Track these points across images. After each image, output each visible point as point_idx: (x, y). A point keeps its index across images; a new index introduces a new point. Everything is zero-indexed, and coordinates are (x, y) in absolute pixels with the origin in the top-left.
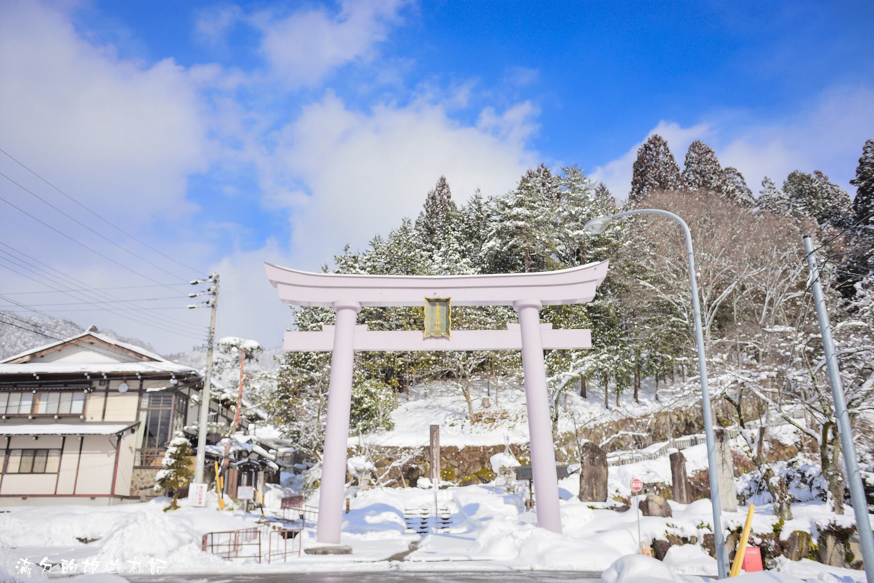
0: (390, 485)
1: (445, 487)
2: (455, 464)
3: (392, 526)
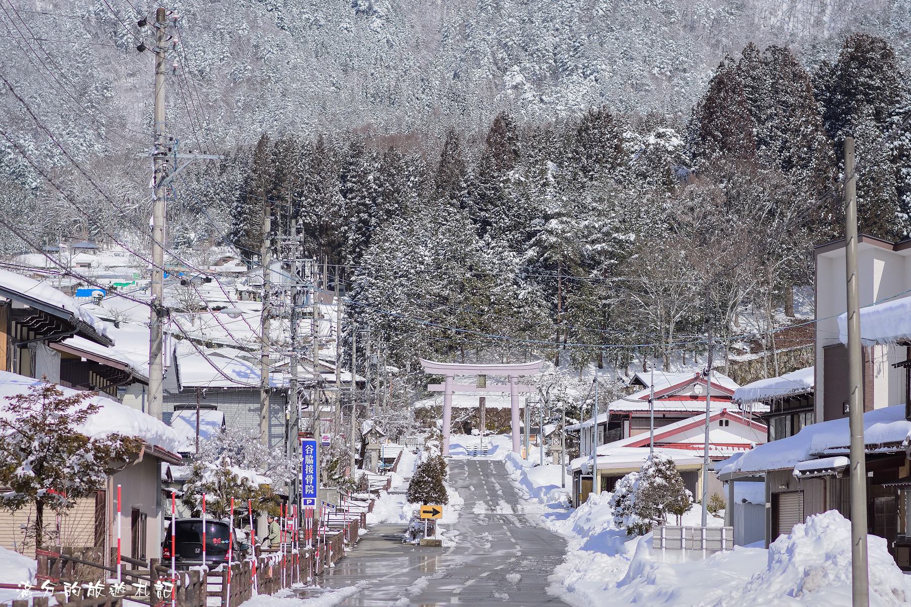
1: (487, 435)
3: (462, 453)
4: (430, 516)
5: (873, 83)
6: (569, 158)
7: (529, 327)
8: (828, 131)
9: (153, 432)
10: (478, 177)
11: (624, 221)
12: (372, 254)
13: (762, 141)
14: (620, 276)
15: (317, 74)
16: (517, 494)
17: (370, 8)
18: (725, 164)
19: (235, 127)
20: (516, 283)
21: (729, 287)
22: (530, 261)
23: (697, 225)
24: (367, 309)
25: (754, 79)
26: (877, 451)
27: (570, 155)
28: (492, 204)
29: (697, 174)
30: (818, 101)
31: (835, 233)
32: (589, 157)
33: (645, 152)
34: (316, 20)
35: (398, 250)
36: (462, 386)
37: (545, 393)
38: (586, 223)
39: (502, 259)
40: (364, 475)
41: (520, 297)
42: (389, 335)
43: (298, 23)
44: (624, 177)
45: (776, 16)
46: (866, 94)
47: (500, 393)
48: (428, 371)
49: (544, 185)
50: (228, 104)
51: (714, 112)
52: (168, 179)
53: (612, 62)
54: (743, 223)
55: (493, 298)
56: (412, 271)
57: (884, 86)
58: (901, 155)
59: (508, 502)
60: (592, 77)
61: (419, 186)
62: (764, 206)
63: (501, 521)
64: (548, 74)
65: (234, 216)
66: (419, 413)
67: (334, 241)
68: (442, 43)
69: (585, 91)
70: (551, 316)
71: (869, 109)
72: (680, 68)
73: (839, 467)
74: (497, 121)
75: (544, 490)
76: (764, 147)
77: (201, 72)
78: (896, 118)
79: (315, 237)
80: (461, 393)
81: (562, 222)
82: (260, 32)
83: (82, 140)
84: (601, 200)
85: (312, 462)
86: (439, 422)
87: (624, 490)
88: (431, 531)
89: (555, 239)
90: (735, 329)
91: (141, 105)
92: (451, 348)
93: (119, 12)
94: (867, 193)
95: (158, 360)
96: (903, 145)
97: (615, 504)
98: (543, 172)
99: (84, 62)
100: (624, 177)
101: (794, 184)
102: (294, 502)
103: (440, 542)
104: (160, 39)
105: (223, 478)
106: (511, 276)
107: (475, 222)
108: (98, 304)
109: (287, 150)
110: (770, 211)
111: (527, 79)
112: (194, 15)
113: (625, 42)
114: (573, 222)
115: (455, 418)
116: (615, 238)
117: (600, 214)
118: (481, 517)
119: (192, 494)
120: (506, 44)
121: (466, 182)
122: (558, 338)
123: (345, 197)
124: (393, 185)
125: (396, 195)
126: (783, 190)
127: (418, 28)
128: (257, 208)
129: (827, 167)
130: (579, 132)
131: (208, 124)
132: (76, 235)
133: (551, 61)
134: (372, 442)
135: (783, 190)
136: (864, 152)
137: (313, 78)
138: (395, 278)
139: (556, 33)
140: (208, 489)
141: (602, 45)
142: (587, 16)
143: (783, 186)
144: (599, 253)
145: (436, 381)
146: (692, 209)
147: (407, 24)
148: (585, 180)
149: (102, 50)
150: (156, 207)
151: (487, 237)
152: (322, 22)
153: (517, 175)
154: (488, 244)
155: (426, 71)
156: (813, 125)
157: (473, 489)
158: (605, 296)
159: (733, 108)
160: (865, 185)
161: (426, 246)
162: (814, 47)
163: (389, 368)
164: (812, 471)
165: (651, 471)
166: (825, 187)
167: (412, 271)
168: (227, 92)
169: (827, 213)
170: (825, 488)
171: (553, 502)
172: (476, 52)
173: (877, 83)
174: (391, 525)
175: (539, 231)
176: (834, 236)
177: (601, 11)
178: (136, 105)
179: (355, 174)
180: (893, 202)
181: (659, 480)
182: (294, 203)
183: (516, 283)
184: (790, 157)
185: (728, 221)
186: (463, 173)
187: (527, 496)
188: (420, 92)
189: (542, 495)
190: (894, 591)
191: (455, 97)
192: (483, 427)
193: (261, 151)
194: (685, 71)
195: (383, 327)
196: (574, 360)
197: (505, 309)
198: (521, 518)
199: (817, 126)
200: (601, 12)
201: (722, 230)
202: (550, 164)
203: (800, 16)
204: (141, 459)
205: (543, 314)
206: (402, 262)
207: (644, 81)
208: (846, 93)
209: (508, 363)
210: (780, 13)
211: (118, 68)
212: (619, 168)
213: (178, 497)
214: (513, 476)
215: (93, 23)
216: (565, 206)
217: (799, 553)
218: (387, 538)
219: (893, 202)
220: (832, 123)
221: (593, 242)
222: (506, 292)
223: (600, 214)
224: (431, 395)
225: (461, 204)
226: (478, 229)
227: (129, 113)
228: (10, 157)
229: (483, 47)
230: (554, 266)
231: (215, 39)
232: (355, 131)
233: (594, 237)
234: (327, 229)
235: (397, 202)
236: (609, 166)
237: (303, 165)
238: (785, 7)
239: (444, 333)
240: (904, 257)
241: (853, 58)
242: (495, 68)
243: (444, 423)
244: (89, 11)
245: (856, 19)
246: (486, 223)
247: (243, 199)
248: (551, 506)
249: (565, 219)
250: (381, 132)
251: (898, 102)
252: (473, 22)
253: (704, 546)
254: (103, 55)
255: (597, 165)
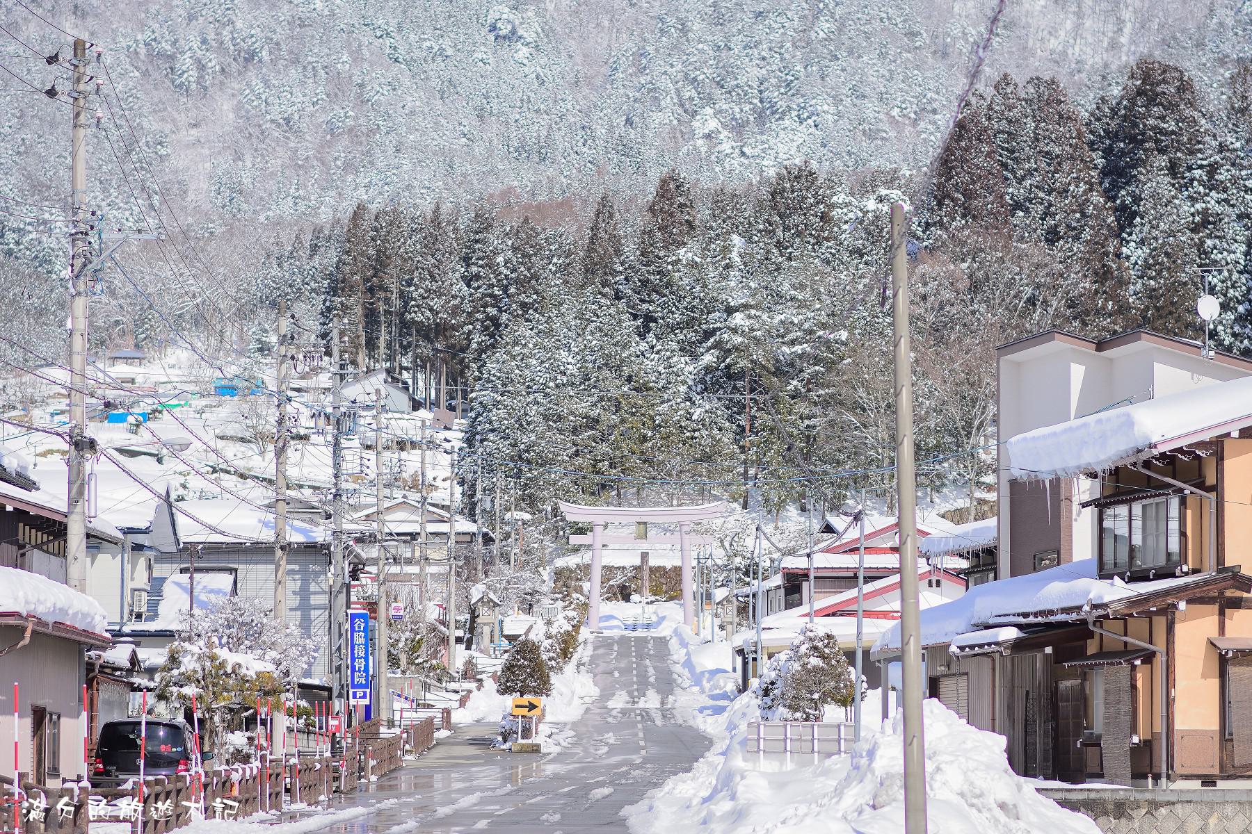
0: (608, 599)
1: (652, 602)
2: (663, 581)
4: (525, 711)
5: (1166, 126)
6: (760, 231)
7: (706, 458)
8: (1107, 191)
9: (49, 604)
10: (637, 259)
11: (833, 315)
12: (498, 362)
13: (1017, 206)
14: (828, 387)
15: (443, 122)
16: (675, 680)
17: (513, 32)
18: (968, 237)
19: (333, 194)
20: (689, 399)
21: (974, 401)
22: (708, 369)
23: (931, 318)
24: (491, 436)
25: (1010, 122)
26: (1052, 619)
27: (761, 227)
28: (657, 293)
29: (931, 250)
30: (1094, 150)
31: (1117, 328)
32: (786, 229)
33: (861, 222)
34: (442, 50)
35: (532, 355)
36: (616, 536)
37: (728, 546)
38: (782, 317)
39: (672, 367)
40: (471, 657)
41: (695, 417)
42: (521, 470)
43: (417, 54)
44: (834, 255)
45: (1056, 38)
46: (1157, 141)
47: (669, 546)
48: (570, 518)
49: (727, 267)
50: (323, 164)
51: (953, 168)
52: (90, 266)
53: (837, 100)
54: (994, 315)
55: (658, 420)
56: (552, 384)
57: (1181, 129)
58: (1205, 223)
59: (658, 692)
60: (810, 121)
61: (564, 270)
62: (1021, 292)
63: (639, 718)
64: (751, 118)
65: (322, 313)
66: (559, 574)
67: (453, 346)
68: (610, 79)
69: (801, 141)
70: (736, 441)
71: (1163, 161)
72: (929, 108)
73: (1009, 641)
74: (664, 182)
75: (707, 675)
76: (1021, 214)
77: (287, 120)
78: (1197, 173)
79: (432, 342)
80: (617, 546)
81: (750, 317)
82: (366, 66)
83: (127, 213)
84: (802, 287)
85: (363, 641)
86: (586, 586)
87: (773, 675)
88: (526, 733)
89: (740, 340)
90: (983, 457)
91: (208, 165)
92: (604, 486)
93: (176, 41)
94: (1159, 273)
95: (78, 509)
96: (1208, 209)
97: (761, 693)
98: (726, 250)
99: (130, 109)
100: (834, 255)
101: (1061, 262)
102: (340, 696)
103: (539, 746)
104: (78, 80)
105: (208, 664)
106: (683, 388)
107: (635, 317)
108: (136, 433)
109: (391, 224)
110: (1029, 300)
111: (724, 126)
112: (277, 44)
113: (855, 73)
114: (765, 317)
115: (609, 580)
116: (820, 337)
117: (801, 305)
118: (614, 713)
119: (167, 685)
120: (695, 79)
121: (622, 264)
122: (746, 472)
123: (469, 286)
124: (529, 270)
125: (534, 282)
126: (1046, 270)
127: (579, 59)
128: (352, 301)
129: (1106, 239)
130: (773, 194)
131: (297, 190)
132: (118, 341)
133: (756, 101)
134: (484, 615)
135: (1046, 270)
136: (1155, 219)
137: (437, 126)
138: (528, 393)
139: (762, 63)
140: (187, 679)
141: (823, 79)
142: (804, 41)
143: (1046, 265)
144: (801, 356)
145: (581, 531)
146: (924, 298)
147: (564, 54)
148: (781, 259)
149: (155, 93)
150: (75, 304)
151: (650, 337)
152: (450, 52)
153: (690, 255)
154: (652, 347)
155: (588, 116)
156: (1086, 183)
157: (616, 674)
158: (804, 416)
159: (980, 161)
160: (1157, 263)
161: (569, 350)
162: (1104, 78)
163: (518, 515)
164: (972, 647)
165: (803, 649)
166: (1104, 266)
167: (552, 384)
168: (322, 147)
169: (1106, 300)
170: (994, 669)
171: (717, 691)
172: (654, 90)
173: (1171, 126)
174: (489, 724)
175: (720, 329)
176: (1115, 332)
177: (821, 33)
178: (200, 166)
179: (481, 254)
180: (1195, 284)
181: (814, 661)
182: (402, 295)
183: (689, 399)
184: (1056, 226)
185: (973, 313)
186: (618, 253)
187: (686, 683)
188: (580, 144)
189: (705, 682)
190: (1002, 806)
191: (625, 149)
192: (646, 592)
193: (356, 226)
194: (934, 111)
195: (512, 459)
196: (767, 500)
197: (677, 434)
198: (666, 713)
199: (1091, 184)
200: (822, 35)
201: (965, 325)
202: (737, 240)
203: (1089, 37)
204: (27, 640)
205: (726, 440)
206: (537, 370)
207: (881, 126)
208: (1133, 139)
209: (679, 505)
210: (1062, 33)
211: (176, 115)
212: (826, 244)
213: (149, 690)
214: (675, 657)
215: (142, 57)
216: (753, 295)
217: (881, 757)
218: (474, 742)
219: (1195, 284)
220: (1113, 180)
221: (792, 343)
222: (676, 411)
223: (801, 305)
224: (576, 549)
225: (616, 293)
226: (638, 327)
227: (192, 177)
228: (31, 236)
229: (664, 83)
230: (741, 375)
231: (305, 76)
232: (492, 196)
233: (792, 336)
234: (445, 330)
235: (536, 293)
236: (813, 241)
237: (412, 245)
238: (1069, 25)
239: (594, 466)
240: (1111, 360)
241: (1140, 93)
242: (680, 111)
243: (592, 586)
244: (136, 41)
245: (1163, 40)
246: (649, 318)
247: (334, 290)
248: (713, 697)
249: (753, 312)
250: (525, 198)
251: (1200, 151)
252: (650, 49)
253: (816, 749)
254: (156, 100)
255: (797, 240)
